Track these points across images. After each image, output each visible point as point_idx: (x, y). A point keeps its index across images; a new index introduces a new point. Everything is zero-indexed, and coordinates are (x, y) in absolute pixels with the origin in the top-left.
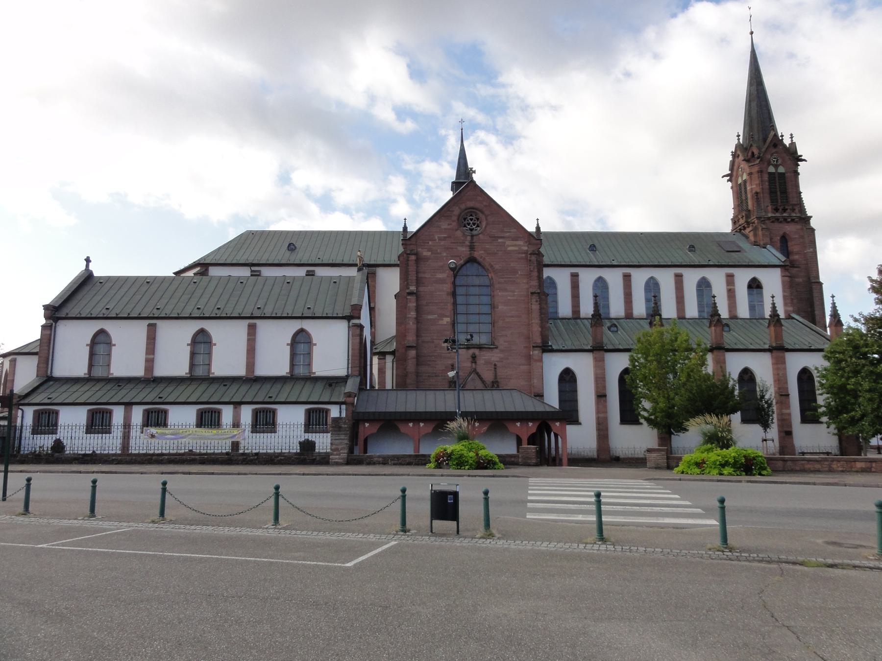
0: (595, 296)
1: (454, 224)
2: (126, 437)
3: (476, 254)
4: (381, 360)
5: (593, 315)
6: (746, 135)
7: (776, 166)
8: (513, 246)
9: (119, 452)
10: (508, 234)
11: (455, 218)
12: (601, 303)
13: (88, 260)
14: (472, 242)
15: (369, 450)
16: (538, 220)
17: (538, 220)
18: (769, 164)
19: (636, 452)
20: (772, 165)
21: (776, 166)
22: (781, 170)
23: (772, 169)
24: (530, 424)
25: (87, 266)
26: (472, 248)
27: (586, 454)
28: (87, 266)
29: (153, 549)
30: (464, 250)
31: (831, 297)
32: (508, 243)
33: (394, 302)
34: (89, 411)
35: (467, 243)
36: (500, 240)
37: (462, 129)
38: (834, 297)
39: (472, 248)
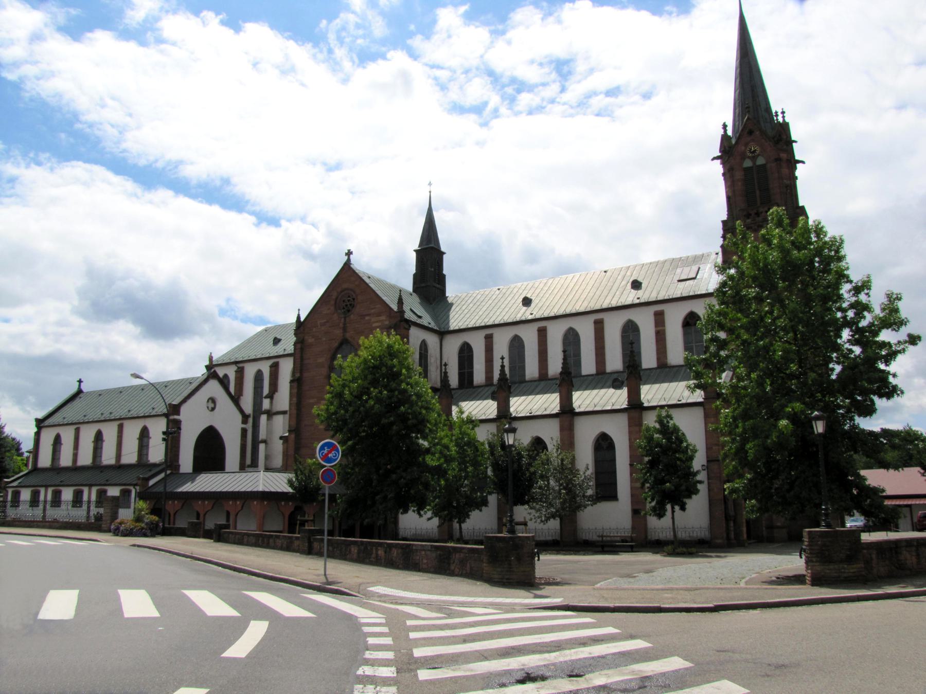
0: (564, 351)
1: (332, 308)
2: (45, 510)
3: (348, 335)
4: (336, 437)
5: (561, 373)
6: (737, 124)
7: (754, 159)
8: (377, 322)
9: (41, 520)
10: (373, 311)
11: (333, 302)
12: (571, 361)
13: (80, 381)
14: (345, 324)
15: (176, 523)
16: (299, 310)
17: (299, 310)
18: (743, 157)
19: (475, 534)
20: (749, 157)
21: (754, 159)
22: (760, 161)
23: (748, 163)
24: (290, 503)
25: (80, 385)
26: (345, 329)
27: (695, 535)
28: (80, 385)
29: (629, 601)
30: (338, 332)
31: (78, 381)
32: (373, 319)
33: (288, 385)
34: (32, 491)
35: (341, 325)
36: (367, 318)
37: (430, 192)
38: (82, 382)
39: (345, 329)
